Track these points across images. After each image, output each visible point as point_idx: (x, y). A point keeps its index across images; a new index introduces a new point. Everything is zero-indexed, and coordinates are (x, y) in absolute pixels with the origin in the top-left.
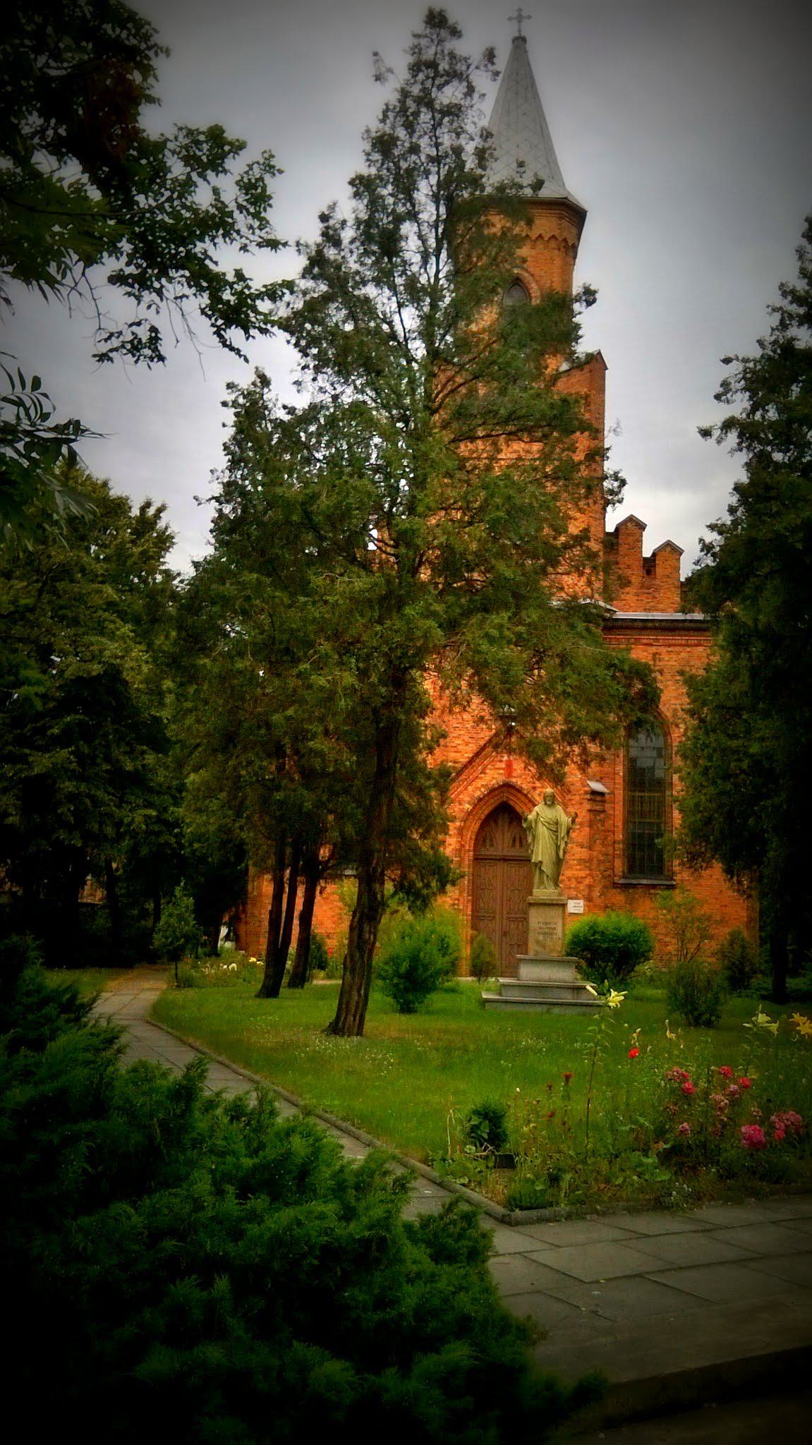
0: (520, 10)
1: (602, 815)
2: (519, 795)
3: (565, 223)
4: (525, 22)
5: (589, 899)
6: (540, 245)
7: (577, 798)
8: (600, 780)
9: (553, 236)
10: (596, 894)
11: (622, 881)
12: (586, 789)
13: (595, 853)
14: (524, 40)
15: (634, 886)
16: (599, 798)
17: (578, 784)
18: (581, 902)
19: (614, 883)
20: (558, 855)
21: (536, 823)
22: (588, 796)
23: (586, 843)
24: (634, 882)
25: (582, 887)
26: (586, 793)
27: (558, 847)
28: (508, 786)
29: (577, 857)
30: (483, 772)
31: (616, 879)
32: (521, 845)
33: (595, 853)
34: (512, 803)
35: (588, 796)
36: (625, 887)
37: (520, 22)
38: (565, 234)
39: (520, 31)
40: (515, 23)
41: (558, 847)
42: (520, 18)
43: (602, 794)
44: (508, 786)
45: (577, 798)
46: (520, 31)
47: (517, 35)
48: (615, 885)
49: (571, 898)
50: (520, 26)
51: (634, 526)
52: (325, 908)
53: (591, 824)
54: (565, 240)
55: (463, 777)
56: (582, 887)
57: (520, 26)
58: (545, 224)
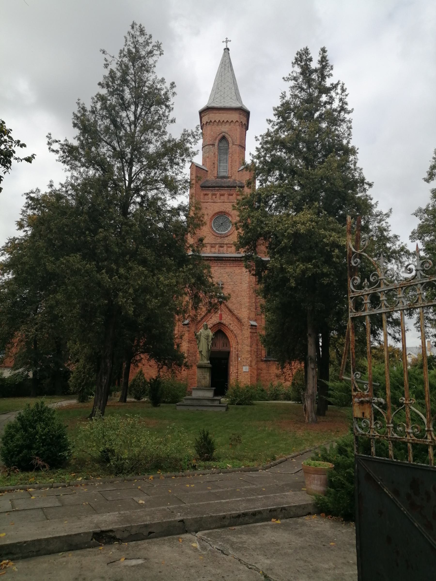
0: (227, 38)
1: (256, 334)
2: (225, 327)
3: (241, 116)
4: (229, 42)
5: (251, 366)
6: (232, 124)
7: (246, 328)
8: (256, 320)
9: (237, 121)
10: (253, 363)
11: (265, 359)
12: (249, 324)
13: (253, 349)
14: (228, 49)
15: (269, 361)
16: (254, 327)
17: (246, 322)
18: (248, 367)
19: (262, 360)
20: (208, 348)
21: (200, 336)
22: (250, 327)
23: (249, 345)
24: (270, 359)
25: (248, 361)
26: (249, 325)
27: (208, 345)
28: (220, 324)
29: (246, 350)
30: (211, 318)
31: (262, 358)
32: (226, 346)
33: (253, 349)
34: (222, 330)
35: (250, 327)
36: (266, 361)
37: (227, 43)
38: (242, 120)
39: (227, 46)
40: (225, 43)
41: (208, 345)
42: (227, 41)
43: (256, 326)
44: (220, 324)
45: (246, 328)
46: (227, 46)
47: (226, 47)
48: (262, 361)
49: (244, 366)
50: (227, 44)
51: (9, 255)
52: (152, 371)
53: (251, 337)
54: (241, 122)
55: (204, 320)
56: (248, 361)
57: (227, 44)
58: (235, 117)
